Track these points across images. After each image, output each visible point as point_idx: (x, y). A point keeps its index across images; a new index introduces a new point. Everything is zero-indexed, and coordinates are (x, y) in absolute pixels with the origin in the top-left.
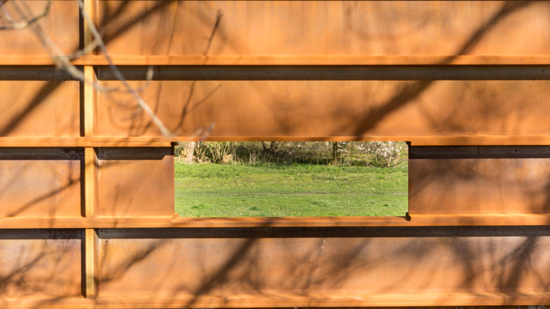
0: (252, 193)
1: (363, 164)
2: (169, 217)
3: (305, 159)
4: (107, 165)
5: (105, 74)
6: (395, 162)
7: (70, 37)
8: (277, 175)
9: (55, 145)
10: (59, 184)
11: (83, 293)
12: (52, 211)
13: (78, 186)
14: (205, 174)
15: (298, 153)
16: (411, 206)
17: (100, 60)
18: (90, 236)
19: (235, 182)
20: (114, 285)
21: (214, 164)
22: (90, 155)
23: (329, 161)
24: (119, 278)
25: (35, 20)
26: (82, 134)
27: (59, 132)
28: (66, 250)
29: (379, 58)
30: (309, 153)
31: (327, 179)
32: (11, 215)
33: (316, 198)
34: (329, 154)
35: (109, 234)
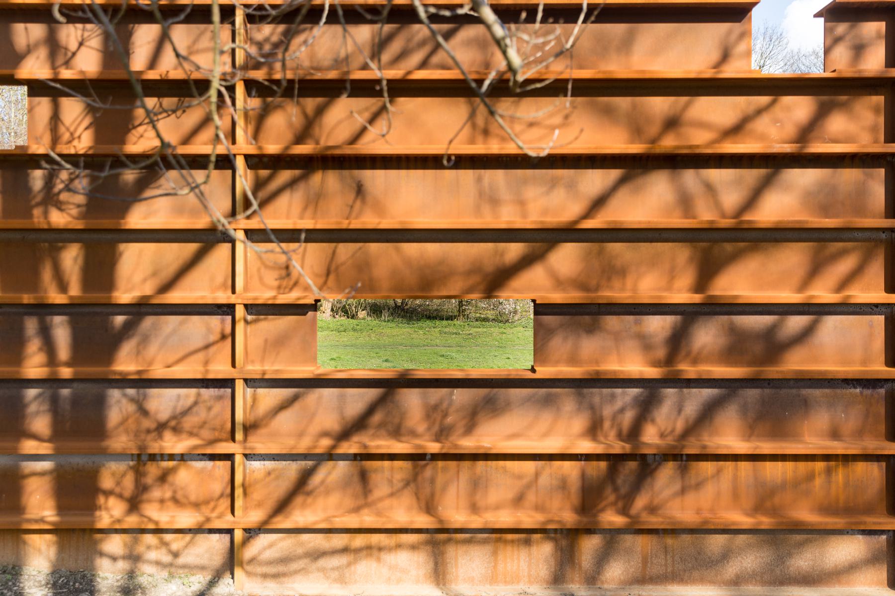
0: (384, 346)
1: (486, 320)
2: (312, 368)
3: (433, 316)
4: (255, 321)
5: (255, 237)
6: (516, 318)
7: (227, 204)
8: (408, 330)
9: (209, 301)
10: (213, 338)
11: (233, 439)
12: (206, 363)
13: (229, 340)
14: (342, 329)
15: (427, 310)
16: (535, 361)
17: (254, 224)
18: (239, 385)
19: (369, 336)
20: (262, 431)
21: (350, 319)
22: (240, 312)
23: (455, 317)
24: (266, 425)
25: (197, 186)
26: (234, 292)
27: (214, 290)
28: (220, 398)
29: (508, 222)
30: (436, 310)
31: (454, 333)
32: (169, 367)
33: (444, 351)
34: (456, 310)
35: (256, 384)
